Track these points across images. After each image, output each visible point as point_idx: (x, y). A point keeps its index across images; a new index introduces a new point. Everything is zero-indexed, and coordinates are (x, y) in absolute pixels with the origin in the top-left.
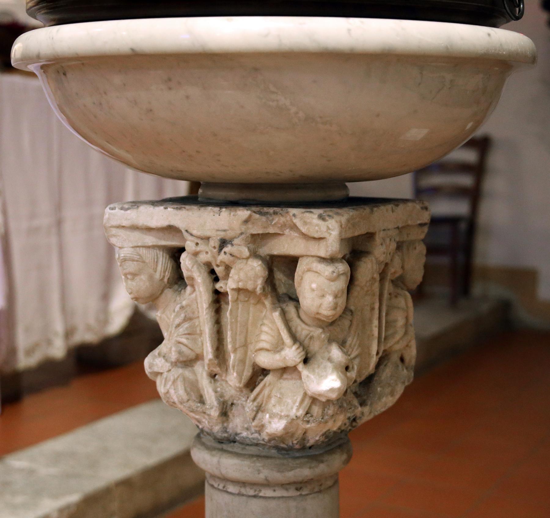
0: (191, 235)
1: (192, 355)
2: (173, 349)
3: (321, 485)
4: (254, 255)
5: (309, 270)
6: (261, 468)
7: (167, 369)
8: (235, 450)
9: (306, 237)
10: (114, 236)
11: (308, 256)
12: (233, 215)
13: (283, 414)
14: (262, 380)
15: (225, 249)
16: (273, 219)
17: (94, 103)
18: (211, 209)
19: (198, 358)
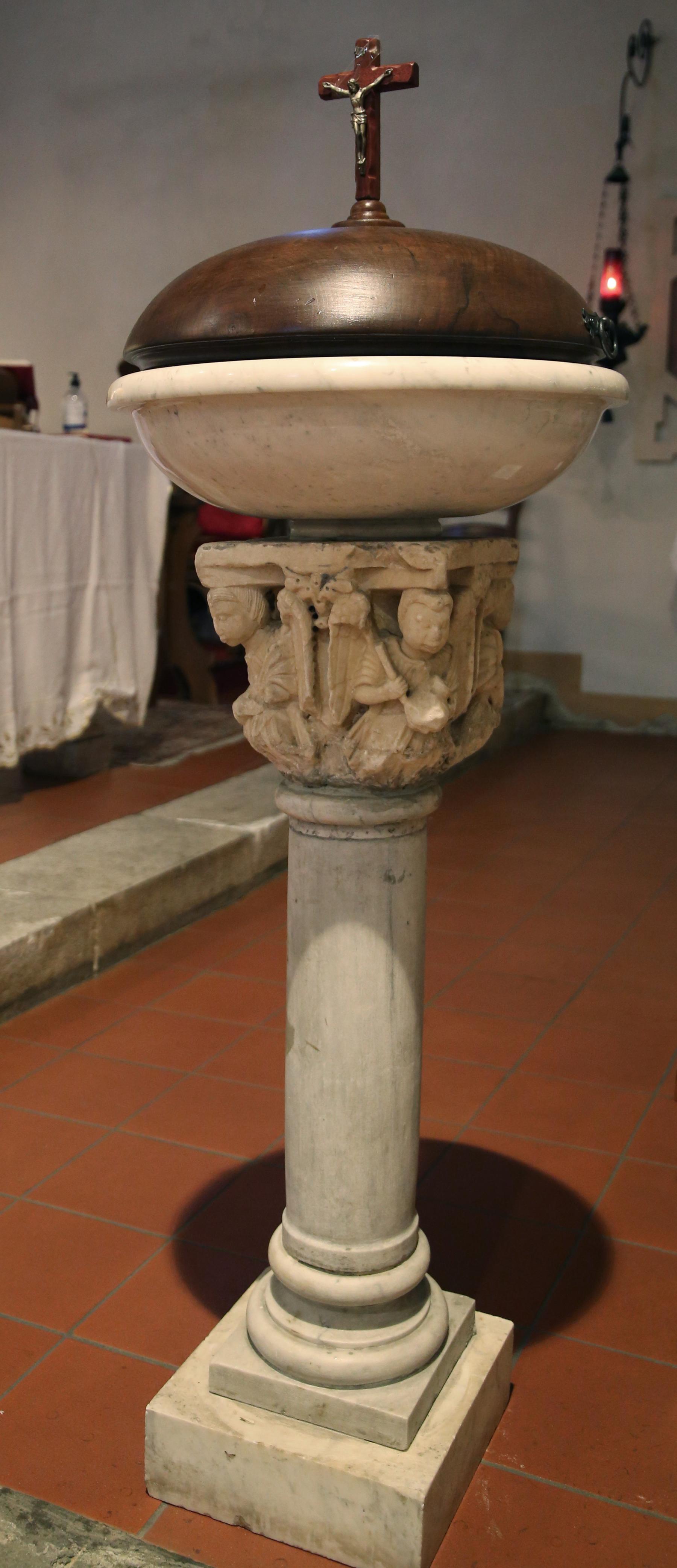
0: (292, 571)
1: (286, 695)
2: (267, 689)
3: (412, 827)
4: (357, 589)
5: (415, 602)
6: (356, 809)
7: (259, 712)
8: (327, 793)
9: (411, 568)
10: (208, 576)
11: (413, 588)
12: (338, 550)
13: (383, 749)
14: (358, 718)
15: (328, 585)
16: (377, 554)
17: (207, 441)
18: (313, 545)
19: (292, 698)
